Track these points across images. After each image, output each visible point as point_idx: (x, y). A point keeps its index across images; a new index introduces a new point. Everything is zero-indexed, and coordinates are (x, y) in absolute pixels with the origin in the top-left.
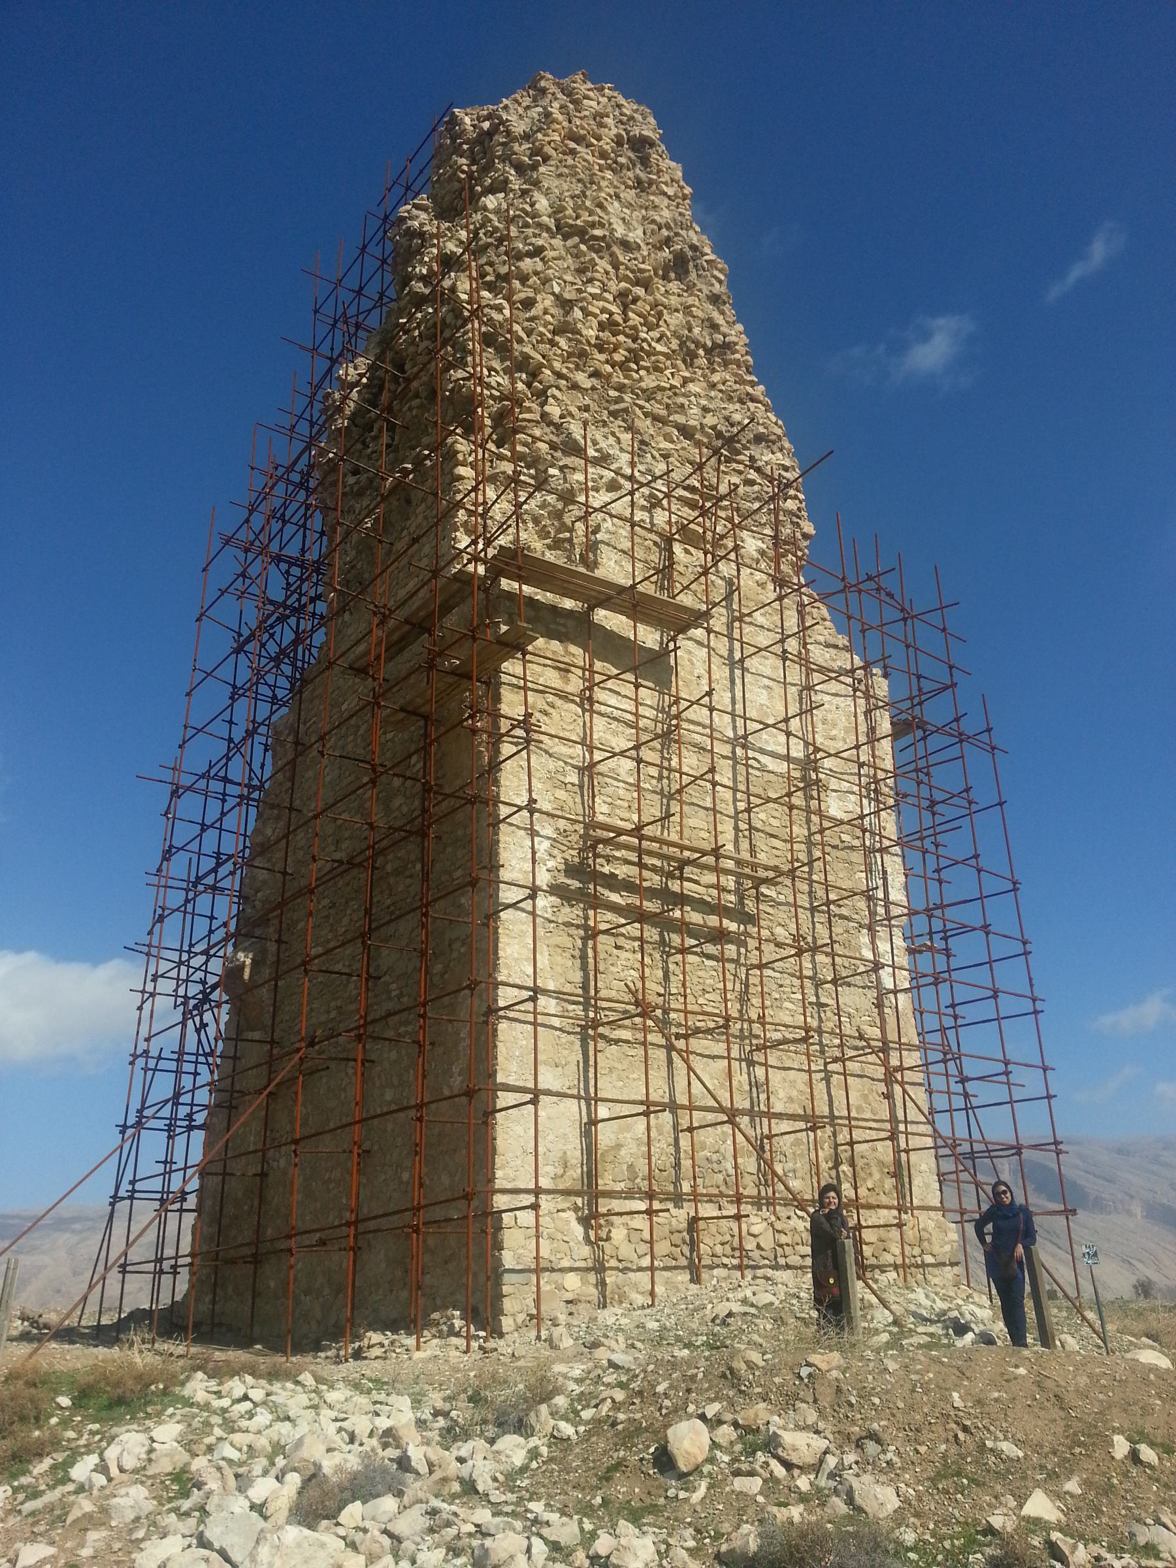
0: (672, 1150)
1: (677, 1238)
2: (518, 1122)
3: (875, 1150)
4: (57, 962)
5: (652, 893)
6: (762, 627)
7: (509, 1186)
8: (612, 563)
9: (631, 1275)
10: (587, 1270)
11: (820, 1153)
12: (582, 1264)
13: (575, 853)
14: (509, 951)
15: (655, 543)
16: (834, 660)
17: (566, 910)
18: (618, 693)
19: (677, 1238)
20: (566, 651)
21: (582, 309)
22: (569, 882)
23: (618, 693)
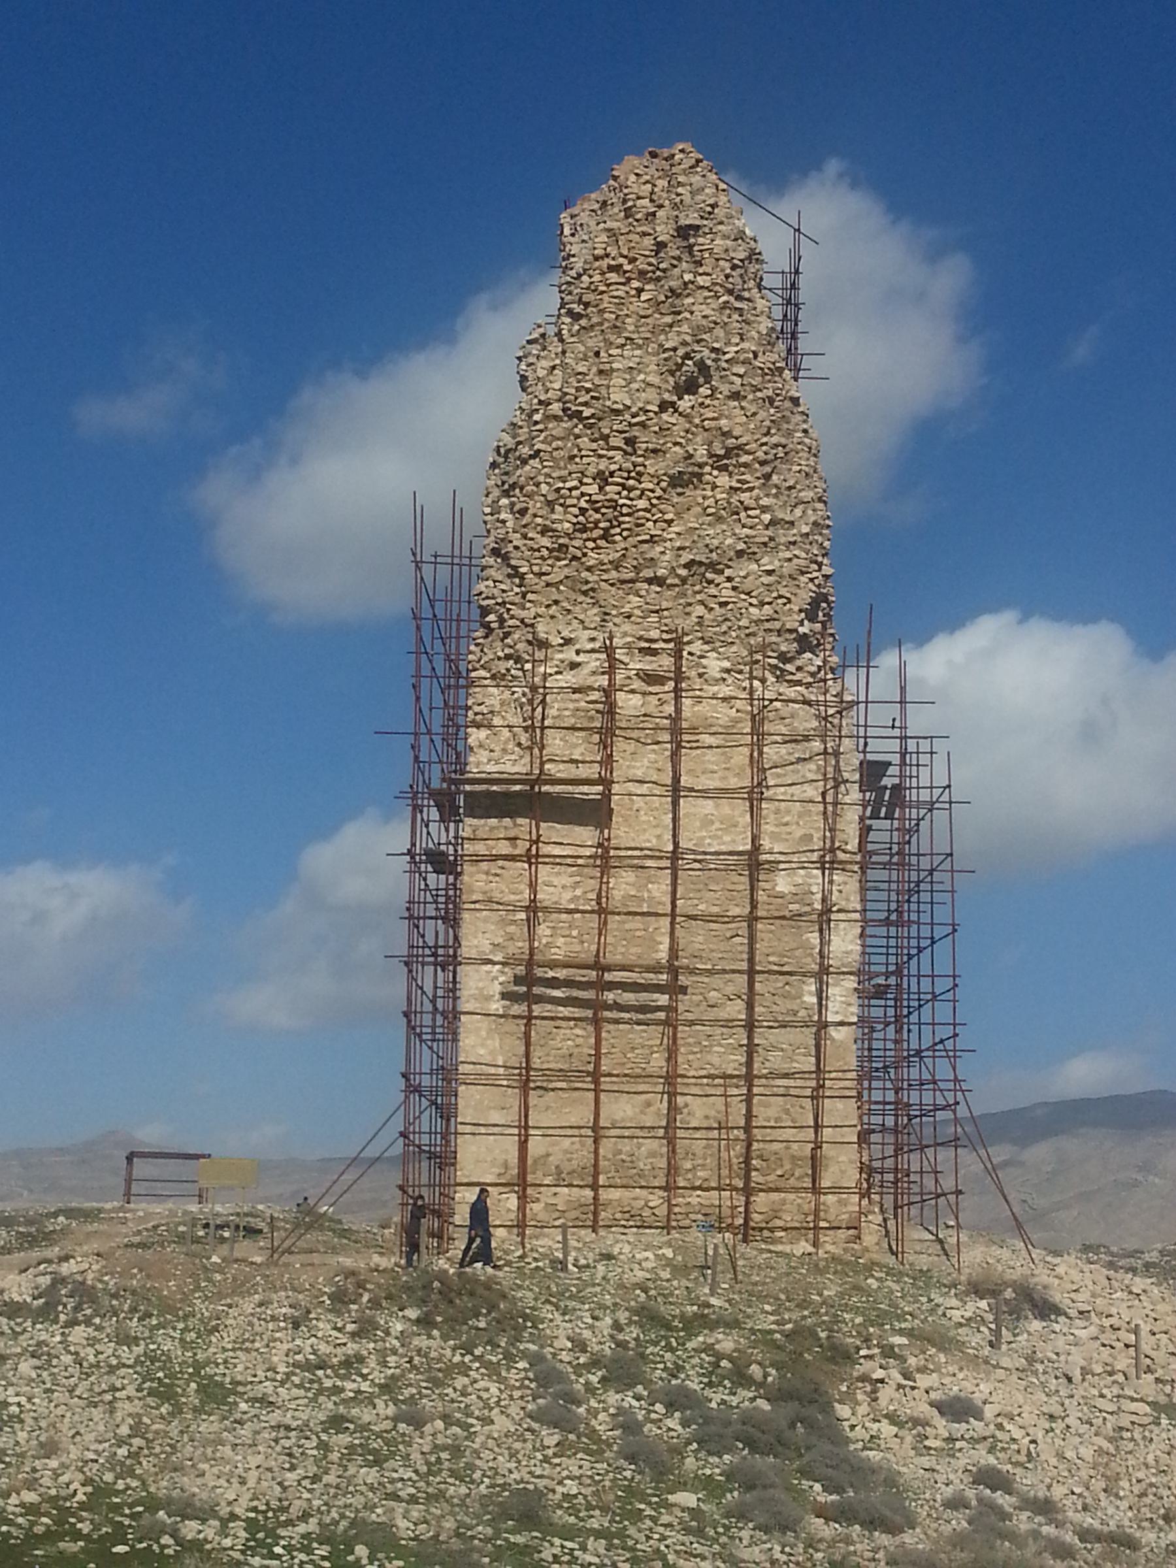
0: (592, 1156)
1: (585, 1209)
2: (877, 1244)
3: (787, 1148)
4: (451, 339)
5: (540, 999)
6: (711, 747)
7: (465, 1180)
8: (557, 742)
9: (546, 1230)
10: (513, 1226)
11: (732, 1153)
12: (509, 1223)
13: (523, 968)
14: (467, 1041)
15: (598, 711)
16: (790, 754)
17: (516, 1007)
18: (561, 844)
19: (585, 1209)
20: (515, 825)
21: (561, 505)
22: (516, 988)
23: (561, 844)
